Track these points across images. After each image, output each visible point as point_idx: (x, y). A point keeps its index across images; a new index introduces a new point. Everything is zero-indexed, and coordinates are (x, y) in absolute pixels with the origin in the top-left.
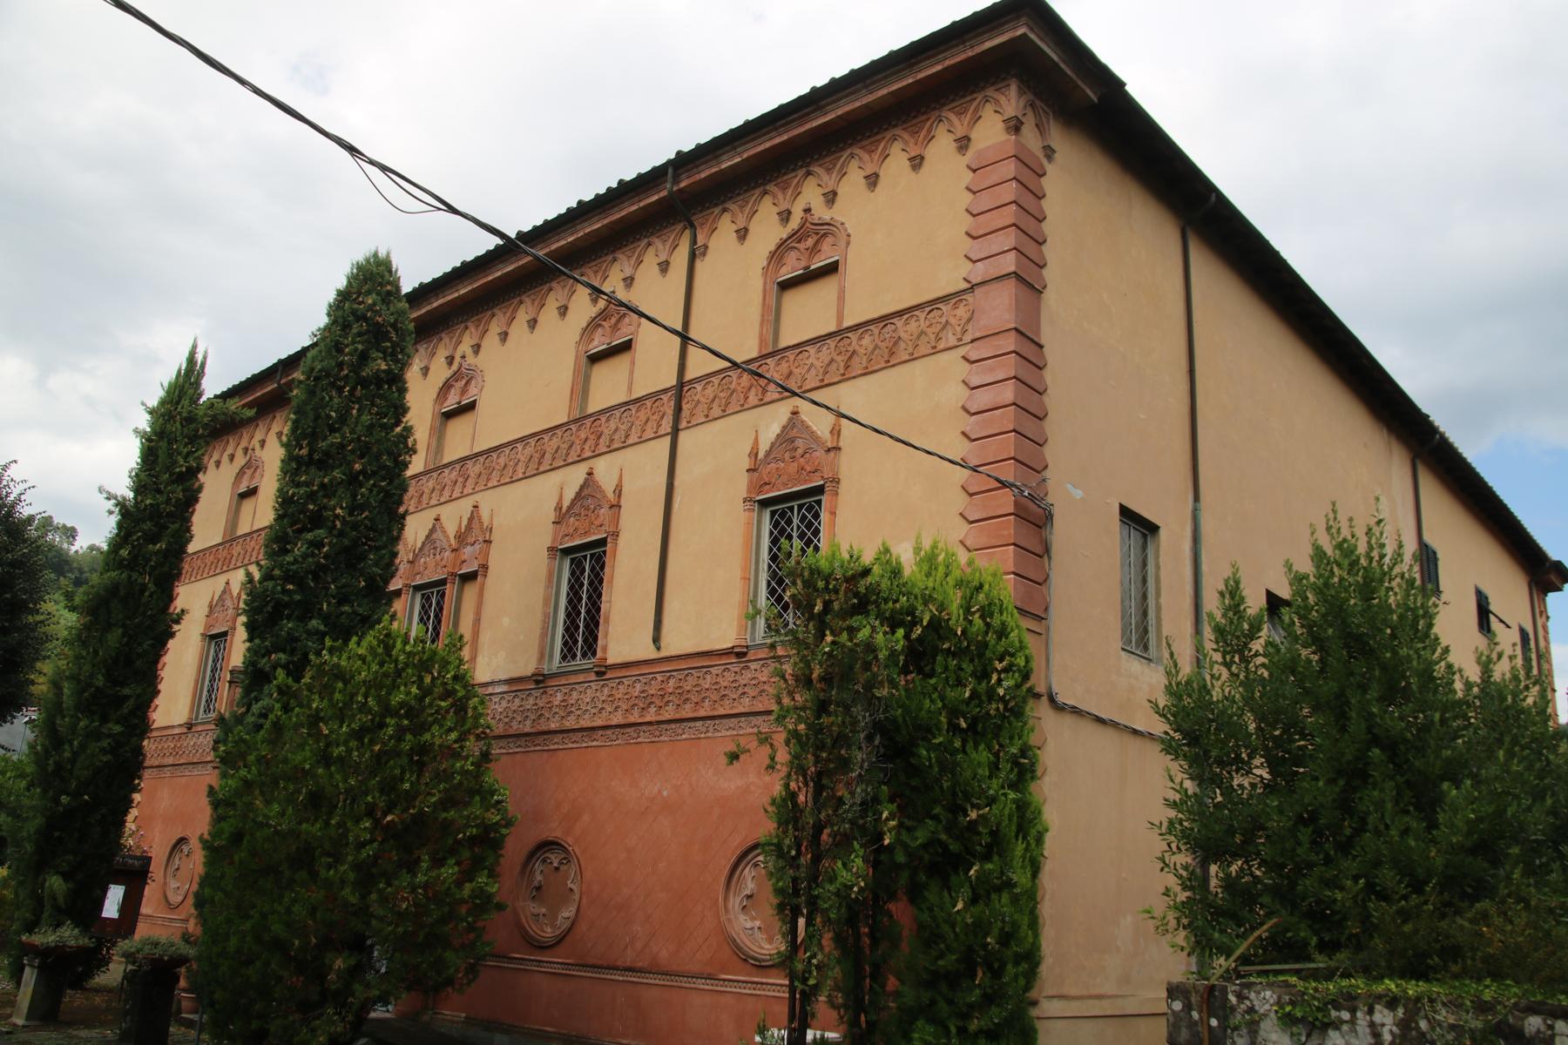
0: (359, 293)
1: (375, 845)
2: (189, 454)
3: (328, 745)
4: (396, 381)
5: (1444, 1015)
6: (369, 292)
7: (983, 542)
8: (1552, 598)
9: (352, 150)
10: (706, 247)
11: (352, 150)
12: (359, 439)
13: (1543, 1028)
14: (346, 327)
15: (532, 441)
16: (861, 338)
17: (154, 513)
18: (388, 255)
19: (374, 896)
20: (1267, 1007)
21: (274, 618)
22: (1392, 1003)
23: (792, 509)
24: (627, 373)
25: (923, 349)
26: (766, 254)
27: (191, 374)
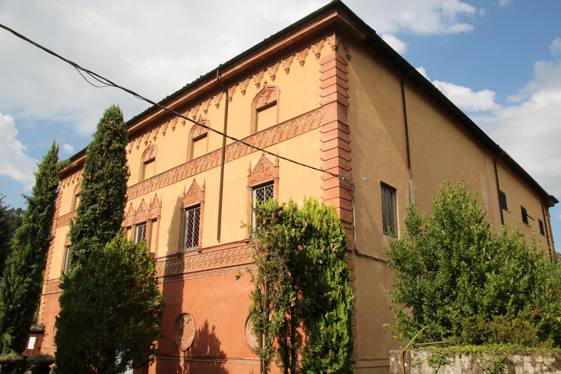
0: (108, 120)
1: (114, 315)
2: (53, 181)
3: (97, 281)
4: (122, 151)
5: (486, 357)
6: (111, 120)
7: (329, 197)
8: (551, 209)
9: (75, 65)
10: (232, 98)
11: (75, 65)
12: (109, 172)
13: (520, 360)
14: (103, 132)
15: (174, 170)
16: (285, 127)
17: (42, 202)
18: (118, 106)
19: (114, 334)
20: (424, 358)
21: (80, 238)
22: (467, 354)
23: (264, 189)
24: (206, 144)
25: (306, 130)
26: (252, 99)
27: (54, 153)
